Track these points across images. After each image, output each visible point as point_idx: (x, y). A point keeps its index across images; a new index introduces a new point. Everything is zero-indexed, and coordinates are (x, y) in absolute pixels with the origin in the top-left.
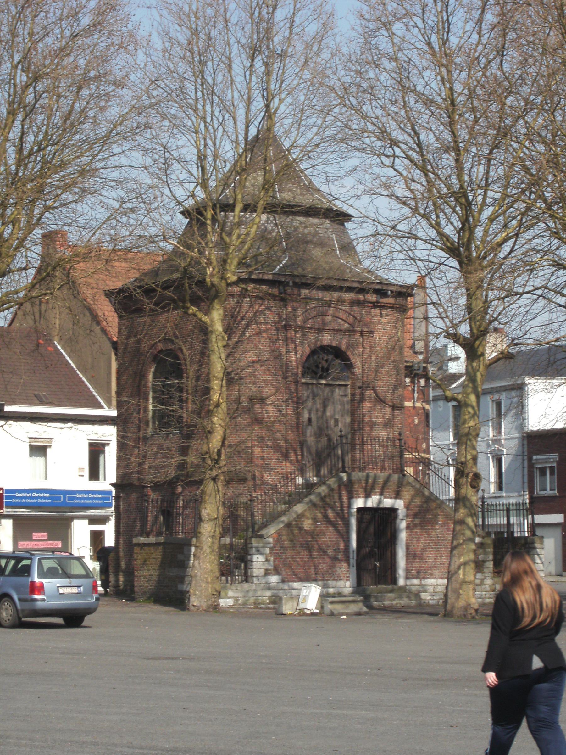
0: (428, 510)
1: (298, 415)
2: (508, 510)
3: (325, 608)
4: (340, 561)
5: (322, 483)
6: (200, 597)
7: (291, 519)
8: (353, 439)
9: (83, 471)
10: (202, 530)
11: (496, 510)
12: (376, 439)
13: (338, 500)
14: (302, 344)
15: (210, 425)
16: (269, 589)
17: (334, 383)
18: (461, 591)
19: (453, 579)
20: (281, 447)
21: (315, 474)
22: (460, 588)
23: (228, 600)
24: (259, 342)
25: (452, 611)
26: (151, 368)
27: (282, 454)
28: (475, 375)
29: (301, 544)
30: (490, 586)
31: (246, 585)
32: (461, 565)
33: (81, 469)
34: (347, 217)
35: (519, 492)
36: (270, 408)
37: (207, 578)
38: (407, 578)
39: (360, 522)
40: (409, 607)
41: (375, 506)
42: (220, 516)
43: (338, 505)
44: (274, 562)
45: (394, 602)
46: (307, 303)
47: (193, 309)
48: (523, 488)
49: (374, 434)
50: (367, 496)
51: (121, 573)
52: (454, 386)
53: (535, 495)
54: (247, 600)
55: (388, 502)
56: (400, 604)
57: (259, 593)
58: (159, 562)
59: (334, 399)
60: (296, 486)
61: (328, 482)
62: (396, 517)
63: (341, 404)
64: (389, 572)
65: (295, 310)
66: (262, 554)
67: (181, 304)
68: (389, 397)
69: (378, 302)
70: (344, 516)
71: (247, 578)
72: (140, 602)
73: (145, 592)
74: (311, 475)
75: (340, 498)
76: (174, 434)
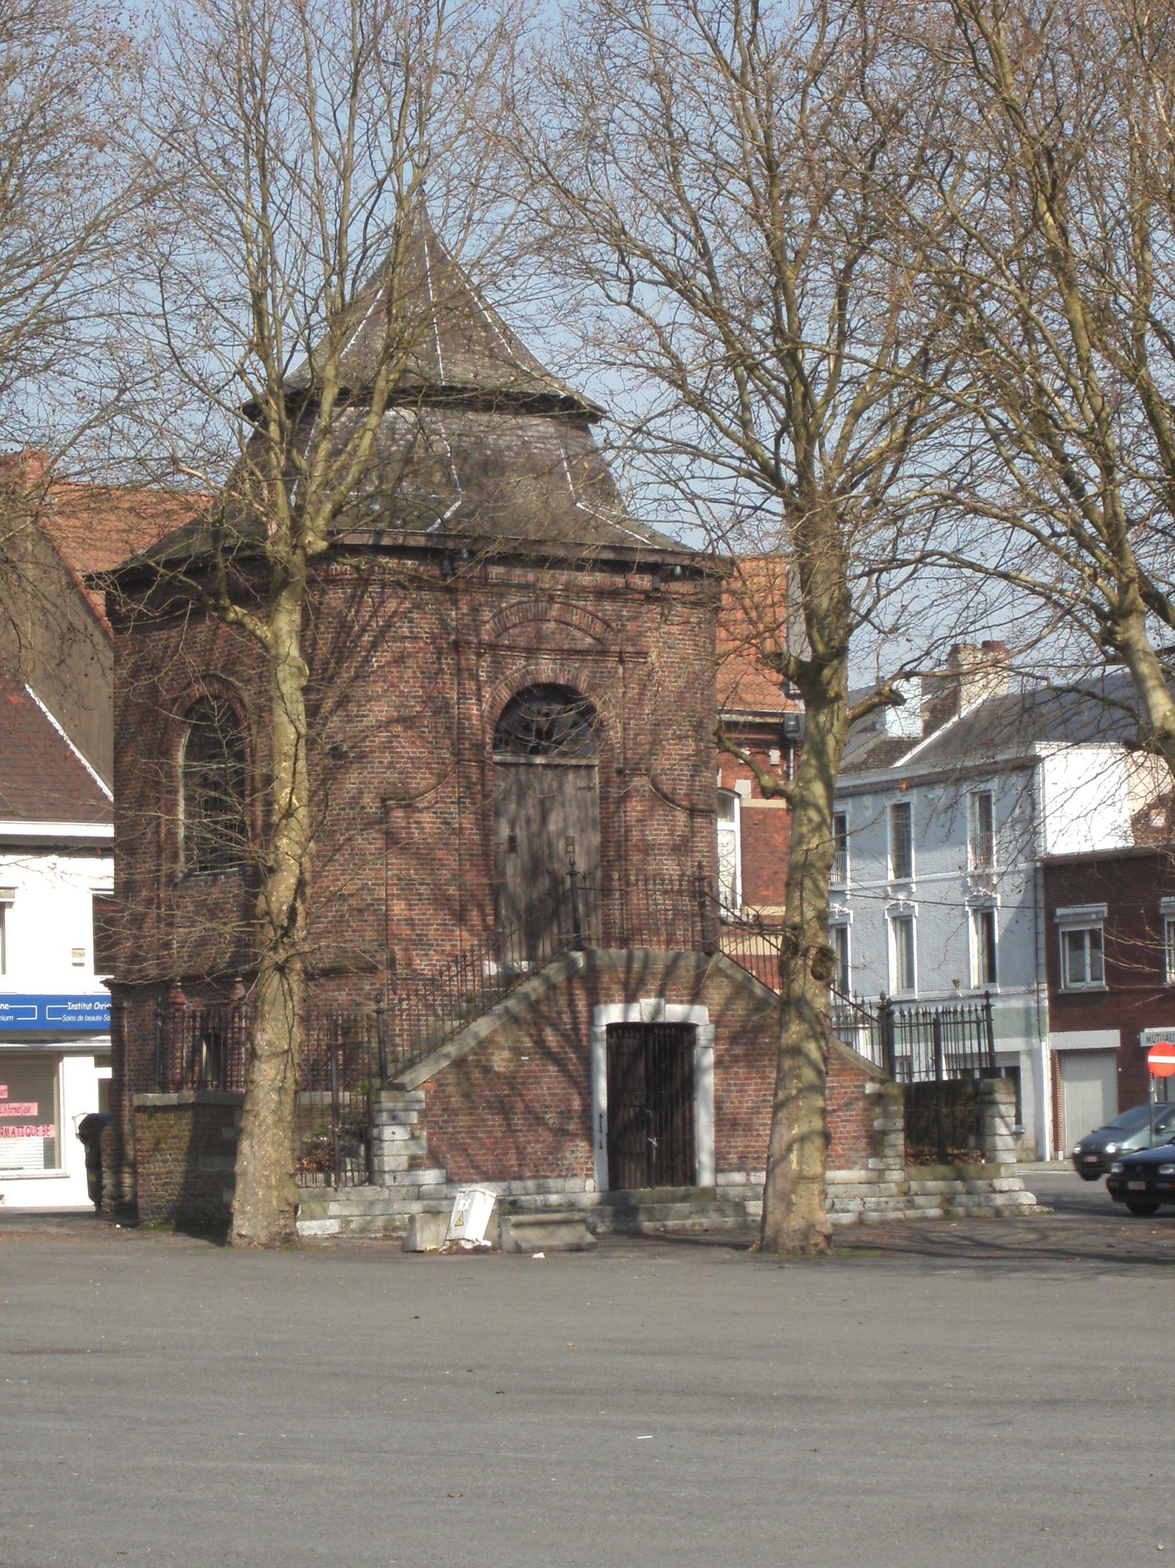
0: (760, 1028)
1: (486, 833)
2: (936, 1024)
3: (504, 1237)
4: (572, 1136)
5: (534, 973)
6: (254, 1216)
7: (466, 1049)
8: (607, 878)
9: (82, 955)
10: (257, 1077)
11: (963, 1023)
12: (658, 877)
13: (566, 1009)
14: (492, 680)
15: (272, 856)
16: (419, 1197)
17: (563, 761)
18: (793, 1197)
19: (777, 1171)
20: (448, 899)
21: (524, 954)
22: (793, 1191)
23: (328, 1222)
24: (400, 678)
25: (775, 1240)
26: (180, 736)
27: (452, 913)
28: (823, 742)
29: (487, 1102)
30: (897, 1184)
31: (368, 1191)
32: (794, 1141)
33: (77, 951)
34: (595, 415)
35: (1029, 984)
36: (426, 817)
37: (267, 1178)
38: (718, 1170)
39: (614, 1053)
40: (718, 1230)
41: (646, 1019)
42: (295, 1047)
43: (566, 1018)
44: (429, 1140)
45: (689, 1222)
46: (502, 596)
47: (236, 612)
48: (1037, 976)
49: (651, 868)
50: (630, 998)
51: (127, 1169)
52: (899, 763)
53: (1062, 989)
54: (368, 1223)
55: (674, 1012)
56: (701, 1225)
57: (396, 1207)
58: (185, 1144)
59: (563, 796)
60: (485, 981)
61: (543, 971)
62: (693, 1042)
63: (579, 807)
64: (681, 1157)
65: (475, 610)
66: (402, 1124)
67: (212, 602)
68: (682, 791)
69: (657, 590)
70: (580, 1041)
71: (371, 1175)
72: (148, 1228)
73: (159, 1208)
74: (516, 956)
75: (571, 1003)
76: (228, 876)
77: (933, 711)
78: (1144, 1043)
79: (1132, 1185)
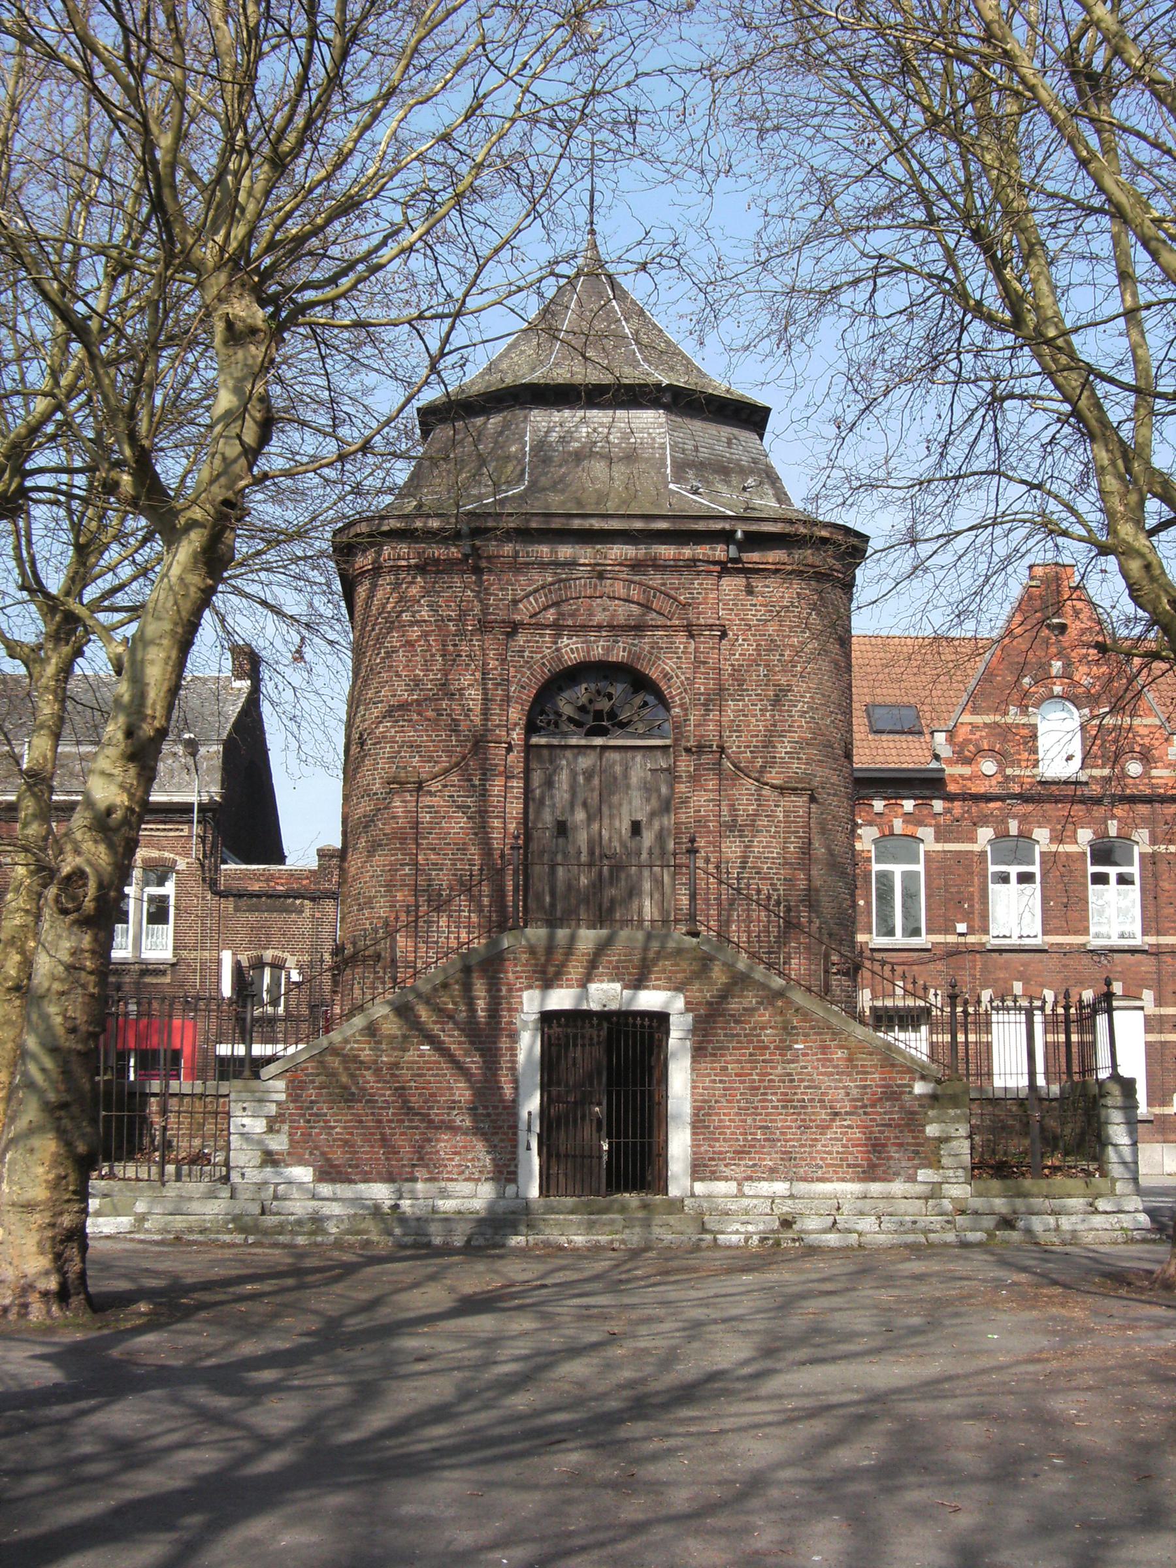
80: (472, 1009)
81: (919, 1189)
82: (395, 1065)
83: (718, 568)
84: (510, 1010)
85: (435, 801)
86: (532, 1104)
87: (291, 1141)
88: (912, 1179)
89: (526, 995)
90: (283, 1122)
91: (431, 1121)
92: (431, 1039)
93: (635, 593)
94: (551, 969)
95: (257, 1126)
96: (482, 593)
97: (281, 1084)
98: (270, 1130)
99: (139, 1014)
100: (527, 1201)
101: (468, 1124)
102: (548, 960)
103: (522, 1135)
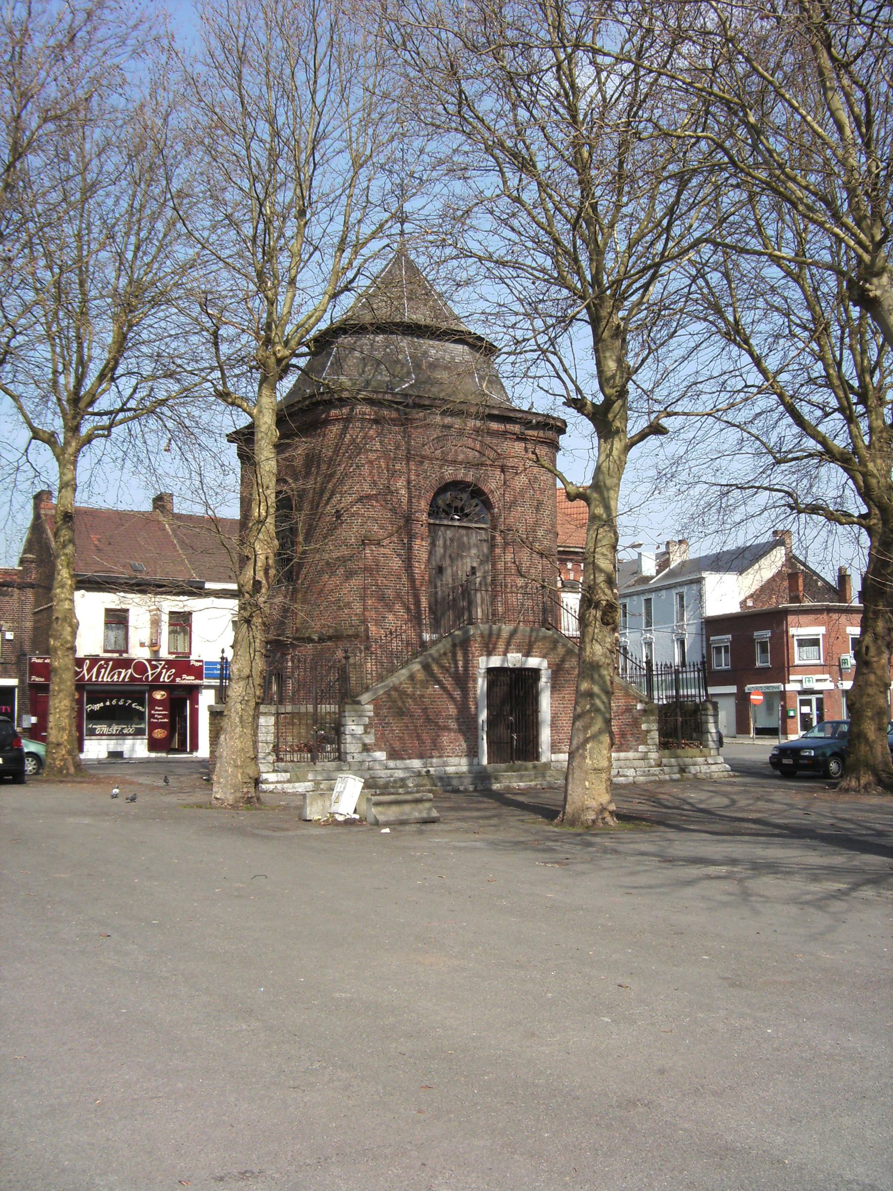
6: (225, 786)
23: (307, 784)
37: (235, 761)
69: (522, 434)
77: (660, 566)
78: (747, 691)
79: (785, 761)
80: (457, 667)
81: (637, 755)
82: (422, 696)
83: (515, 437)
84: (473, 667)
85: (386, 551)
86: (483, 716)
87: (376, 738)
88: (637, 751)
89: (480, 659)
90: (371, 728)
91: (439, 726)
92: (439, 682)
93: (478, 447)
94: (491, 646)
95: (359, 730)
96: (407, 435)
97: (370, 707)
98: (366, 732)
99: (293, 668)
100: (485, 768)
101: (456, 727)
102: (489, 641)
103: (480, 732)
